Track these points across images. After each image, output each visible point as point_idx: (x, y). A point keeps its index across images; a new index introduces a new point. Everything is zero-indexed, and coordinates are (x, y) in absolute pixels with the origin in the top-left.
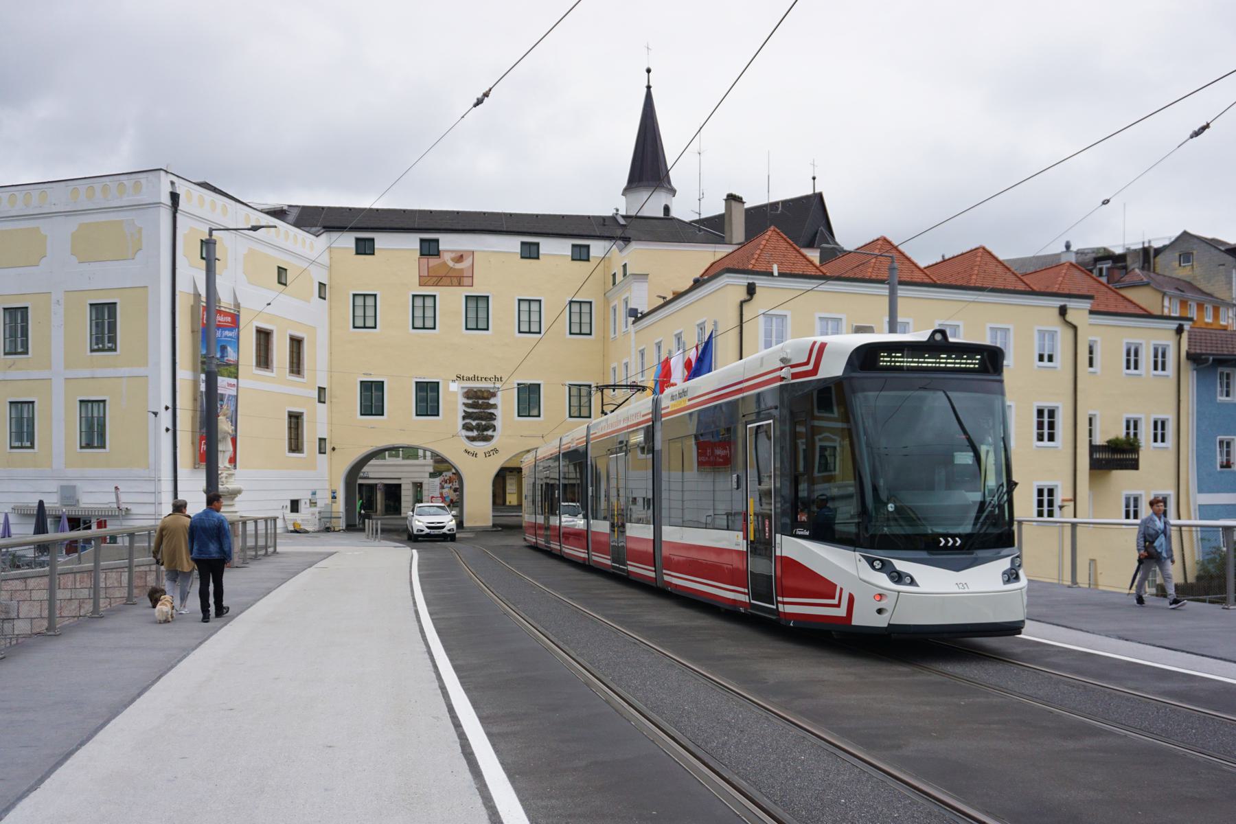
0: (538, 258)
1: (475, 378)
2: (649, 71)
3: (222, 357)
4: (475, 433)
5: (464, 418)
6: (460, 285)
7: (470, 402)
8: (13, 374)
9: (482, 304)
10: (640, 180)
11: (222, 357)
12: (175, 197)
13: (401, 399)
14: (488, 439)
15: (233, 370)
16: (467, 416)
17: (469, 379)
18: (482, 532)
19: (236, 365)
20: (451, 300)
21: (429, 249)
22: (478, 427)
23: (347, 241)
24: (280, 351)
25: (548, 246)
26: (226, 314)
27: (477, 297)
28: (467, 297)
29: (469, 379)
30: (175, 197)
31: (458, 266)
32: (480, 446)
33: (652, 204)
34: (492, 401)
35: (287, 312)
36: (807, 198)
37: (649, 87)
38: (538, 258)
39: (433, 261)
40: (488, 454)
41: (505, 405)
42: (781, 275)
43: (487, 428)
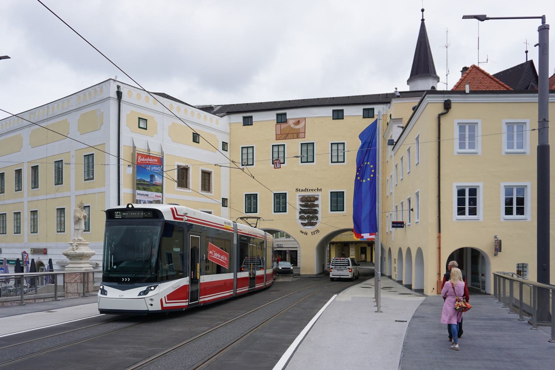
0: (343, 119)
1: (306, 190)
2: (423, 10)
3: (151, 181)
4: (306, 221)
5: (300, 213)
6: (298, 138)
7: (304, 203)
8: (58, 195)
9: (310, 148)
10: (417, 74)
11: (151, 181)
12: (119, 94)
13: (265, 204)
14: (313, 224)
15: (160, 188)
16: (302, 211)
17: (303, 191)
18: (310, 278)
19: (162, 185)
20: (293, 147)
21: (281, 119)
22: (308, 218)
23: (238, 119)
24: (195, 179)
25: (348, 111)
26: (154, 158)
27: (307, 144)
28: (301, 144)
29: (303, 191)
30: (119, 94)
31: (297, 127)
32: (309, 229)
33: (424, 85)
34: (316, 203)
35: (198, 158)
36: (522, 65)
37: (423, 20)
38: (343, 119)
39: (284, 126)
40: (313, 233)
41: (323, 204)
42: (472, 92)
43: (313, 218)
